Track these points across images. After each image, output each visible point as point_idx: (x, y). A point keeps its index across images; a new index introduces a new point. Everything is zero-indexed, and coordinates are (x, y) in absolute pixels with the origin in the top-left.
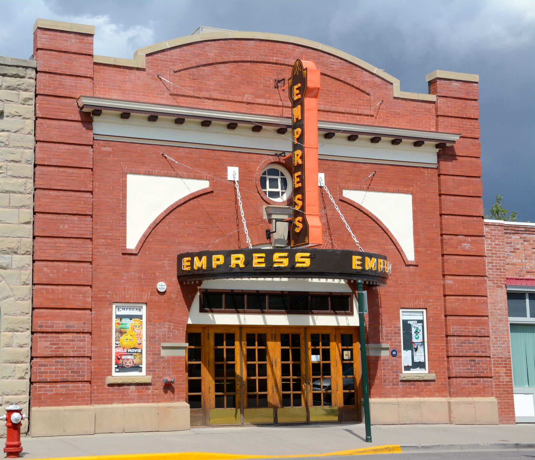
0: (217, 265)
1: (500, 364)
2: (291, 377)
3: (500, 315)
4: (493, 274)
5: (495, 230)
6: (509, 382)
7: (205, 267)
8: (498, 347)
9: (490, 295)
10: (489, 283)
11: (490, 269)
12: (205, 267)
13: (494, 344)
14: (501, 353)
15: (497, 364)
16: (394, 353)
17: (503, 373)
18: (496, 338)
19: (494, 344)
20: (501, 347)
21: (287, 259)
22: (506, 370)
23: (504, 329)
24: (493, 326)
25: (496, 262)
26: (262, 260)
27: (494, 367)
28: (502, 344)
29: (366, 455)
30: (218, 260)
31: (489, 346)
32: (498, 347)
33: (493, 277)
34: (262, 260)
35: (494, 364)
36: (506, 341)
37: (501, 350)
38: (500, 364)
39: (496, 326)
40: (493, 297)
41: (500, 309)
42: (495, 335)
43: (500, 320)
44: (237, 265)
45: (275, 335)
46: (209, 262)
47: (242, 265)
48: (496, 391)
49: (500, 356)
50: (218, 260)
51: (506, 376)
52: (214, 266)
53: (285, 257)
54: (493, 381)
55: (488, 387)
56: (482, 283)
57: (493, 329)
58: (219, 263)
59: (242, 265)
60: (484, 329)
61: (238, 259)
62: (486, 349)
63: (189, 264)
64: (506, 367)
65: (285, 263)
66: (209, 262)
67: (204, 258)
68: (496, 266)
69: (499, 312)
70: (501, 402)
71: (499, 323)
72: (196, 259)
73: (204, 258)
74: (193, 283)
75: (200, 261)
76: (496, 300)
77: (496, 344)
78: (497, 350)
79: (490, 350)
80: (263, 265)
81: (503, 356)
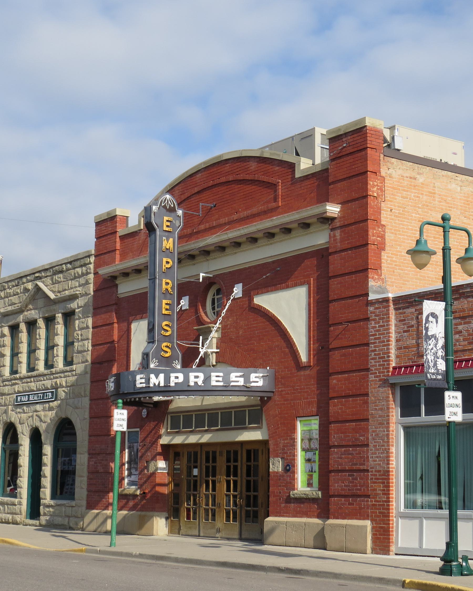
0: (175, 383)
1: (378, 479)
2: (411, 482)
3: (380, 416)
4: (376, 366)
5: (379, 308)
6: (386, 501)
7: (162, 384)
8: (377, 457)
9: (372, 392)
10: (372, 377)
11: (372, 359)
12: (162, 384)
13: (372, 454)
14: (379, 464)
15: (375, 479)
16: (288, 468)
17: (380, 490)
18: (375, 446)
19: (372, 454)
20: (380, 457)
21: (251, 380)
22: (383, 487)
23: (384, 434)
24: (373, 431)
25: (379, 349)
26: (220, 379)
27: (372, 483)
28: (382, 453)
29: (366, 544)
30: (177, 378)
31: (368, 457)
32: (377, 457)
33: (375, 369)
34: (220, 379)
35: (372, 479)
36: (385, 449)
37: (380, 461)
38: (378, 479)
39: (376, 431)
40: (374, 395)
41: (381, 409)
42: (375, 442)
43: (380, 424)
44: (196, 383)
45: (222, 451)
46: (167, 379)
47: (200, 383)
48: (372, 512)
49: (378, 468)
50: (177, 378)
51: (383, 494)
52: (172, 384)
53: (240, 376)
54: (371, 502)
55: (364, 507)
56: (364, 378)
57: (372, 435)
58: (177, 381)
59: (200, 383)
60: (364, 436)
61: (197, 377)
62: (364, 461)
63: (143, 381)
64: (383, 483)
65: (241, 382)
66: (167, 379)
67: (162, 376)
68: (380, 354)
69: (380, 412)
70: (376, 527)
71: (380, 428)
72: (152, 376)
73: (162, 376)
74: (137, 399)
75: (157, 378)
76: (377, 398)
77: (375, 454)
78: (376, 461)
79: (368, 461)
80: (221, 384)
81: (382, 469)
